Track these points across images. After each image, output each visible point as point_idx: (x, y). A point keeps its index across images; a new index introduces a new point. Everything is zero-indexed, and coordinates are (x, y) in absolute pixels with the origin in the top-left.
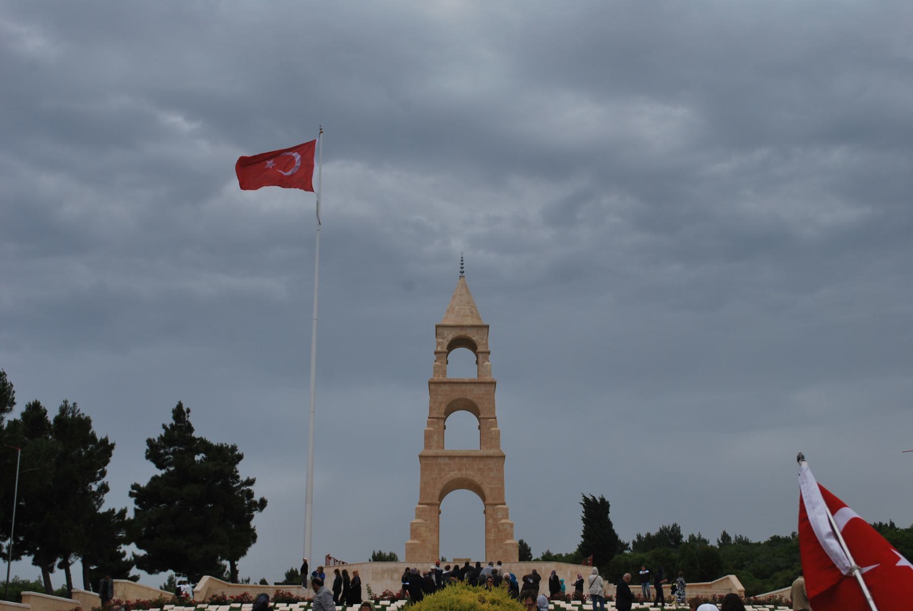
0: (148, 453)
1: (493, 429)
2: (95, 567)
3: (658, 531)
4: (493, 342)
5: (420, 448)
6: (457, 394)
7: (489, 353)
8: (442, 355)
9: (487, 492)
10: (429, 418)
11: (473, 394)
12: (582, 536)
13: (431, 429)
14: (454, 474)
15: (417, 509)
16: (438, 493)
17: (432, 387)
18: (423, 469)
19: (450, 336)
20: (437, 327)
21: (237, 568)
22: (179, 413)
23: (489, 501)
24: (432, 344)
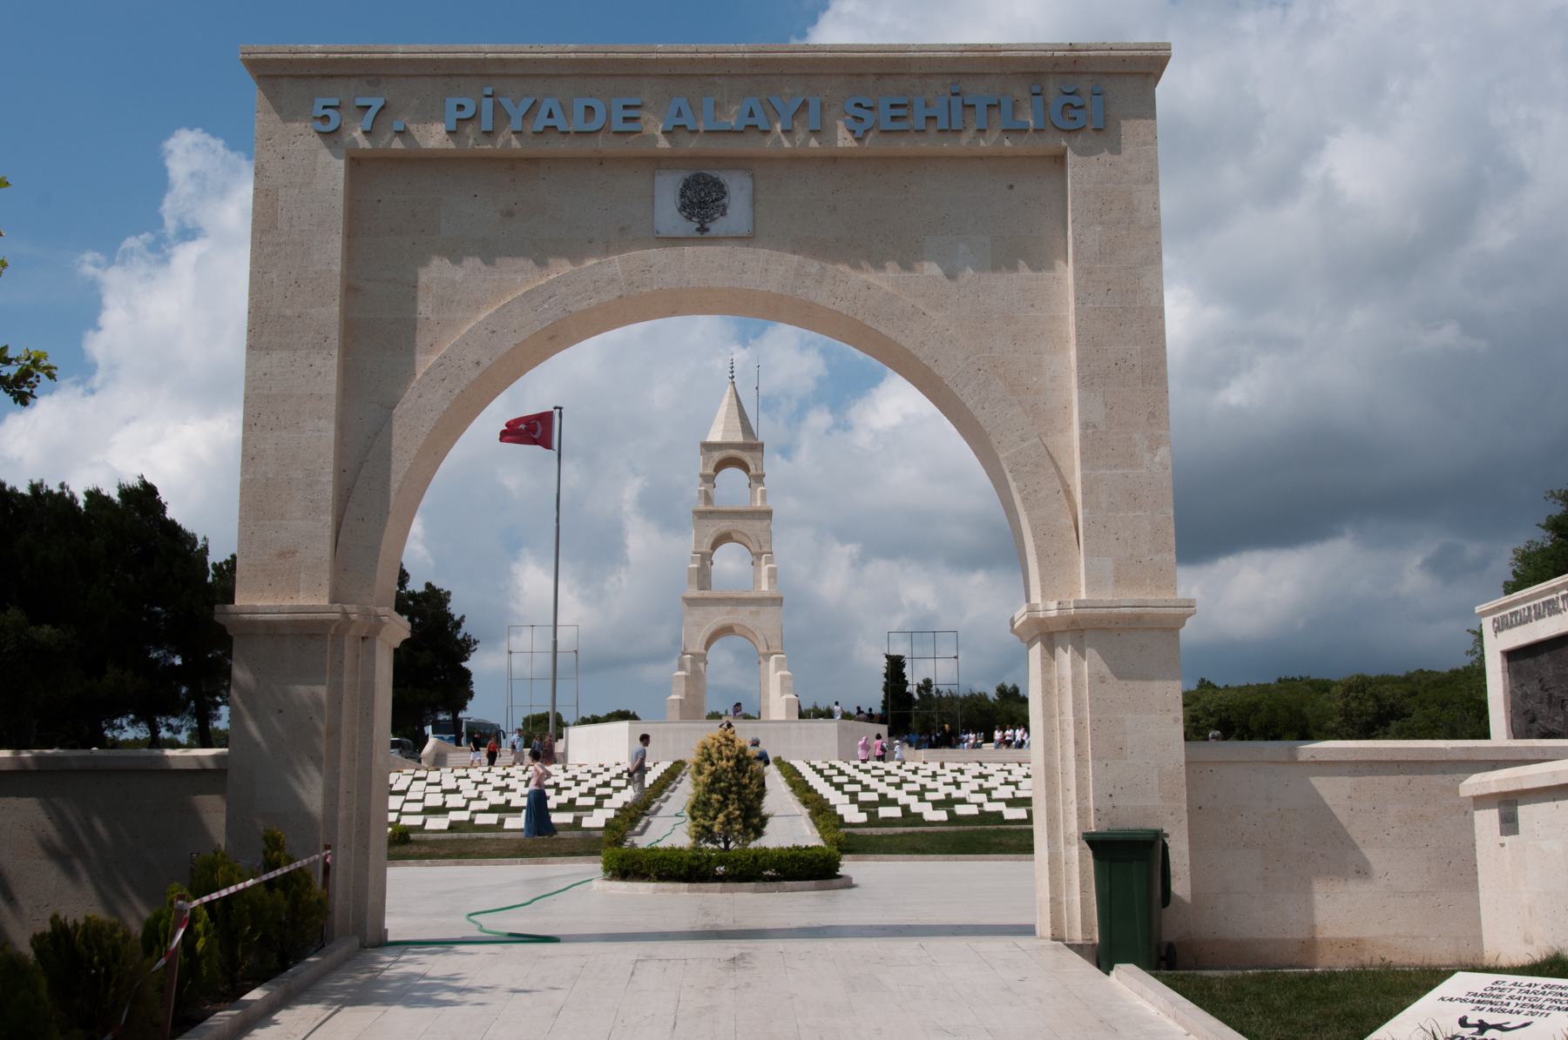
6: (724, 525)
19: (718, 456)
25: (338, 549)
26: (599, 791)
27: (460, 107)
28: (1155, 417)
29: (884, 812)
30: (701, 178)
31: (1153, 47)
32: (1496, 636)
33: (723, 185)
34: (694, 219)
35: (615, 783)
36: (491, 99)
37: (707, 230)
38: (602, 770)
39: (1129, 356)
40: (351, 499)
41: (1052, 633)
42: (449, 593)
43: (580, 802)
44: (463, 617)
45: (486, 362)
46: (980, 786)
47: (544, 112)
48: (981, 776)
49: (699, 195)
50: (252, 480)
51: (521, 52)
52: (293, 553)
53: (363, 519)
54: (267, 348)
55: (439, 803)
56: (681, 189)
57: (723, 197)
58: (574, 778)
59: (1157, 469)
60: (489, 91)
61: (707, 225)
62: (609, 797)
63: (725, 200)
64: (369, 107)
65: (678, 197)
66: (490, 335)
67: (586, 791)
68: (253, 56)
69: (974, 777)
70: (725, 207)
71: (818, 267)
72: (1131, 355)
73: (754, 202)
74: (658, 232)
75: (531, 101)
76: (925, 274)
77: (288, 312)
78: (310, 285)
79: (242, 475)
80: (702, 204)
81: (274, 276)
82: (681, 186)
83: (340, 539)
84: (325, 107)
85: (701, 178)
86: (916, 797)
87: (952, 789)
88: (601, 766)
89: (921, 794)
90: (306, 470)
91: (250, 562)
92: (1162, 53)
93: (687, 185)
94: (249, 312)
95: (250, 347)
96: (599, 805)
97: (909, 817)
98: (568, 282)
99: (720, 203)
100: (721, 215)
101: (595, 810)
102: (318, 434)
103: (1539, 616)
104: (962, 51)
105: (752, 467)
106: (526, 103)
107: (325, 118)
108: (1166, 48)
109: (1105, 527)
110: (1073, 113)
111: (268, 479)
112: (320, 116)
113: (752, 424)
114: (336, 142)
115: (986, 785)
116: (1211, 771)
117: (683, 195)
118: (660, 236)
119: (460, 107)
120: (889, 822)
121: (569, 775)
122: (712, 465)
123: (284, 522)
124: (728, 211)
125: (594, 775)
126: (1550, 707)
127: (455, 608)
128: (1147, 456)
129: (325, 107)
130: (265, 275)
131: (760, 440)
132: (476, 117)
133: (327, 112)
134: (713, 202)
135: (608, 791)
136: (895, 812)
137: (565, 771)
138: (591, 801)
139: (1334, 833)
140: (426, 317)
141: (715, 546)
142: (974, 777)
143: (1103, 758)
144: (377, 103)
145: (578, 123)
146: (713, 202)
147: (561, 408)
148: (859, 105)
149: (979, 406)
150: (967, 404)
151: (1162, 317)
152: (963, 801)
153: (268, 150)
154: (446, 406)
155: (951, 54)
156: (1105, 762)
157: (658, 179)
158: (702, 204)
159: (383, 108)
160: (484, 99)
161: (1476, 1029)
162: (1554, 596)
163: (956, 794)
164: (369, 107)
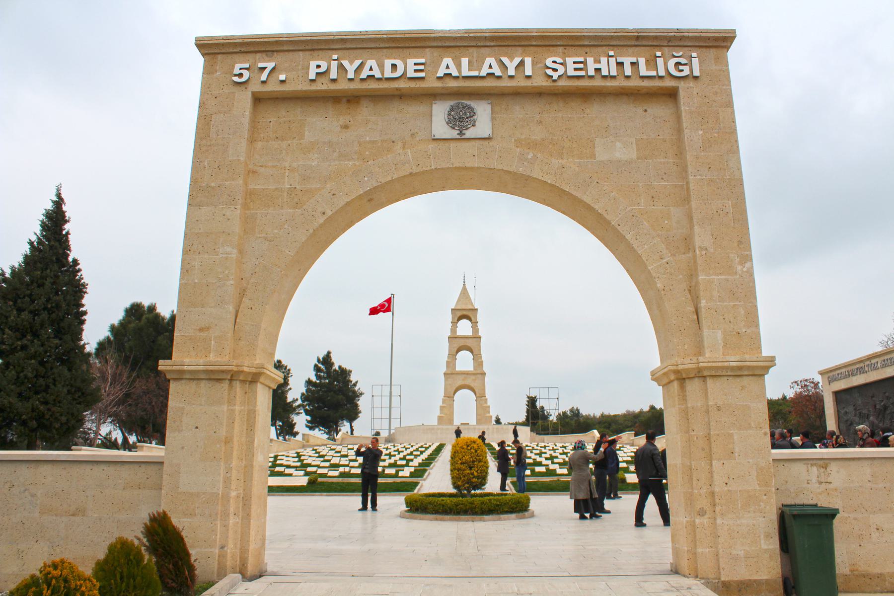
0: (118, 425)
1: (480, 360)
2: (607, 476)
3: (639, 410)
4: (480, 317)
5: (444, 369)
6: (462, 343)
7: (478, 322)
8: (454, 323)
9: (476, 390)
10: (449, 355)
11: (469, 343)
12: (586, 415)
13: (449, 360)
14: (460, 382)
15: (443, 399)
16: (453, 392)
17: (450, 339)
18: (446, 380)
19: (459, 314)
20: (452, 310)
21: (353, 428)
22: (329, 353)
23: (478, 395)
24: (449, 317)
25: (236, 326)
26: (408, 457)
27: (318, 66)
28: (743, 244)
29: (538, 469)
30: (460, 105)
31: (726, 31)
32: (830, 384)
33: (473, 109)
34: (456, 128)
35: (415, 453)
36: (337, 61)
37: (464, 134)
38: (410, 446)
39: (724, 207)
40: (245, 295)
41: (684, 379)
42: (350, 372)
43: (399, 463)
44: (357, 382)
45: (329, 213)
46: (553, 448)
47: (367, 67)
48: (563, 447)
49: (459, 114)
50: (186, 284)
51: (355, 35)
52: (208, 329)
53: (251, 308)
54: (199, 206)
55: (346, 453)
56: (449, 111)
57: (474, 116)
58: (398, 450)
59: (746, 276)
60: (335, 57)
61: (464, 132)
62: (412, 460)
63: (475, 117)
64: (266, 68)
65: (446, 116)
66: (332, 196)
67: (401, 453)
68: (202, 42)
69: (561, 447)
70: (475, 121)
71: (532, 155)
72: (725, 206)
73: (493, 119)
74: (434, 136)
75: (360, 61)
76: (597, 159)
77: (213, 184)
78: (226, 168)
79: (180, 281)
80: (461, 119)
81: (206, 164)
82: (448, 109)
83: (237, 320)
84: (241, 69)
85: (460, 105)
86: (538, 456)
87: (552, 452)
88: (410, 444)
89: (551, 458)
90: (218, 277)
91: (183, 334)
92: (732, 35)
93: (452, 109)
94: (190, 185)
95: (189, 205)
96: (407, 465)
97: (551, 473)
98: (380, 165)
99: (472, 119)
100: (473, 125)
101: (405, 468)
102: (226, 256)
103: (854, 375)
104: (615, 32)
105: (473, 319)
106: (357, 63)
107: (241, 75)
108: (733, 32)
109: (716, 311)
110: (681, 67)
111: (195, 283)
112: (237, 73)
113: (472, 299)
114: (246, 88)
115: (565, 451)
116: (783, 465)
117: (449, 115)
118: (435, 138)
119: (318, 66)
120: (541, 474)
121: (396, 449)
122: (456, 319)
123: (204, 309)
124: (477, 123)
125: (406, 449)
126: (860, 419)
127: (353, 378)
128: (739, 268)
129: (241, 69)
130: (201, 163)
131: (476, 308)
132: (327, 72)
133: (242, 71)
134: (467, 118)
135: (412, 457)
136: (543, 469)
137: (394, 447)
138: (404, 462)
139: (861, 504)
140: (294, 187)
141: (458, 351)
142: (561, 447)
143: (721, 459)
144: (270, 65)
145: (388, 74)
146: (467, 118)
147: (394, 295)
148: (554, 62)
149: (634, 238)
150: (626, 237)
151: (742, 184)
152: (557, 457)
153: (208, 94)
154: (304, 239)
155: (608, 34)
156: (722, 462)
157: (434, 106)
158: (461, 119)
159: (274, 69)
160: (332, 62)
161: (651, 500)
162: (862, 365)
163: (554, 454)
164: (266, 68)
